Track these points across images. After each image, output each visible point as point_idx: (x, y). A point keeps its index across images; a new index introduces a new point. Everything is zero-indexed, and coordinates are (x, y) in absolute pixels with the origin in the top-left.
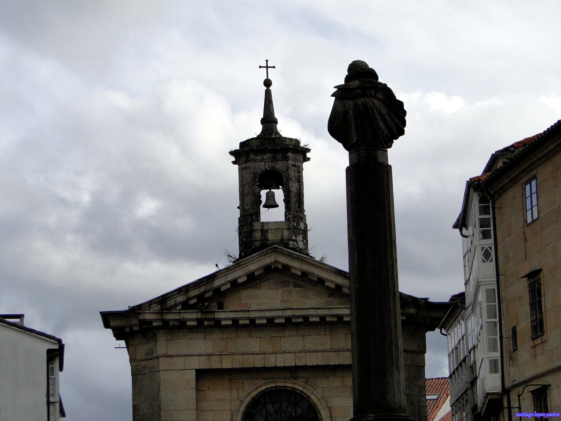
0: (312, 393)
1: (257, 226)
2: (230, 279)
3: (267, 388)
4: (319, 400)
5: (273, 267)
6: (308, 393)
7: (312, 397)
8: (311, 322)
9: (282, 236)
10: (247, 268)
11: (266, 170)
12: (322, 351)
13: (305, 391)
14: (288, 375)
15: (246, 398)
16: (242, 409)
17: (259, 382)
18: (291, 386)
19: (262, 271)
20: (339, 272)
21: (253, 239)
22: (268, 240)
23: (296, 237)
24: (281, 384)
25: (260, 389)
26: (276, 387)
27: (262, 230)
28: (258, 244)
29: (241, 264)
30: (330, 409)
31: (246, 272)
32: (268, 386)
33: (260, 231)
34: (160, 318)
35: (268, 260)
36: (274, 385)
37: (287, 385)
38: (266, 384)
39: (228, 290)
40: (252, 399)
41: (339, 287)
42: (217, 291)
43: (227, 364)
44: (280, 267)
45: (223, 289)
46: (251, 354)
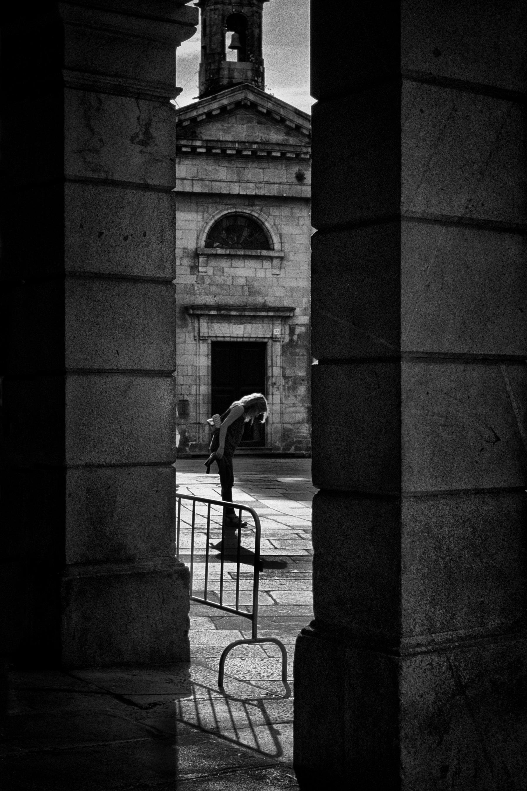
0: (266, 220)
1: (224, 65)
2: (206, 111)
3: (228, 213)
4: (272, 227)
5: (242, 103)
6: (263, 220)
7: (267, 224)
8: (214, 153)
9: (246, 76)
10: (221, 102)
11: (234, 13)
12: (279, 184)
13: (260, 218)
14: (247, 203)
15: (211, 220)
16: (207, 230)
17: (220, 207)
18: (249, 212)
19: (233, 106)
20: (299, 113)
21: (221, 76)
22: (234, 78)
23: (258, 78)
24: (240, 210)
25: (222, 214)
26: (236, 212)
27: (229, 69)
28: (225, 81)
29: (218, 97)
30: (280, 235)
31: (220, 105)
32: (229, 211)
33: (227, 70)
34: (205, 145)
35: (240, 96)
36: (234, 210)
37: (245, 211)
38: (228, 209)
39: (202, 120)
40: (216, 221)
41: (298, 127)
42: (193, 120)
43: (197, 189)
44: (249, 103)
45: (199, 119)
46: (218, 181)
